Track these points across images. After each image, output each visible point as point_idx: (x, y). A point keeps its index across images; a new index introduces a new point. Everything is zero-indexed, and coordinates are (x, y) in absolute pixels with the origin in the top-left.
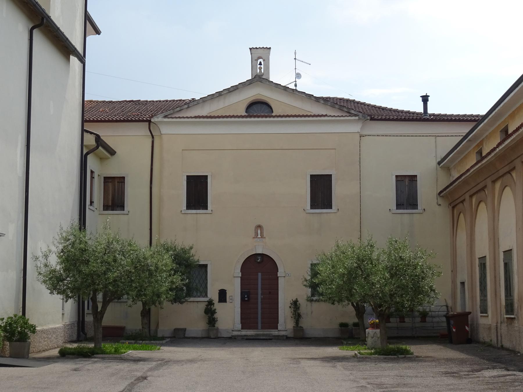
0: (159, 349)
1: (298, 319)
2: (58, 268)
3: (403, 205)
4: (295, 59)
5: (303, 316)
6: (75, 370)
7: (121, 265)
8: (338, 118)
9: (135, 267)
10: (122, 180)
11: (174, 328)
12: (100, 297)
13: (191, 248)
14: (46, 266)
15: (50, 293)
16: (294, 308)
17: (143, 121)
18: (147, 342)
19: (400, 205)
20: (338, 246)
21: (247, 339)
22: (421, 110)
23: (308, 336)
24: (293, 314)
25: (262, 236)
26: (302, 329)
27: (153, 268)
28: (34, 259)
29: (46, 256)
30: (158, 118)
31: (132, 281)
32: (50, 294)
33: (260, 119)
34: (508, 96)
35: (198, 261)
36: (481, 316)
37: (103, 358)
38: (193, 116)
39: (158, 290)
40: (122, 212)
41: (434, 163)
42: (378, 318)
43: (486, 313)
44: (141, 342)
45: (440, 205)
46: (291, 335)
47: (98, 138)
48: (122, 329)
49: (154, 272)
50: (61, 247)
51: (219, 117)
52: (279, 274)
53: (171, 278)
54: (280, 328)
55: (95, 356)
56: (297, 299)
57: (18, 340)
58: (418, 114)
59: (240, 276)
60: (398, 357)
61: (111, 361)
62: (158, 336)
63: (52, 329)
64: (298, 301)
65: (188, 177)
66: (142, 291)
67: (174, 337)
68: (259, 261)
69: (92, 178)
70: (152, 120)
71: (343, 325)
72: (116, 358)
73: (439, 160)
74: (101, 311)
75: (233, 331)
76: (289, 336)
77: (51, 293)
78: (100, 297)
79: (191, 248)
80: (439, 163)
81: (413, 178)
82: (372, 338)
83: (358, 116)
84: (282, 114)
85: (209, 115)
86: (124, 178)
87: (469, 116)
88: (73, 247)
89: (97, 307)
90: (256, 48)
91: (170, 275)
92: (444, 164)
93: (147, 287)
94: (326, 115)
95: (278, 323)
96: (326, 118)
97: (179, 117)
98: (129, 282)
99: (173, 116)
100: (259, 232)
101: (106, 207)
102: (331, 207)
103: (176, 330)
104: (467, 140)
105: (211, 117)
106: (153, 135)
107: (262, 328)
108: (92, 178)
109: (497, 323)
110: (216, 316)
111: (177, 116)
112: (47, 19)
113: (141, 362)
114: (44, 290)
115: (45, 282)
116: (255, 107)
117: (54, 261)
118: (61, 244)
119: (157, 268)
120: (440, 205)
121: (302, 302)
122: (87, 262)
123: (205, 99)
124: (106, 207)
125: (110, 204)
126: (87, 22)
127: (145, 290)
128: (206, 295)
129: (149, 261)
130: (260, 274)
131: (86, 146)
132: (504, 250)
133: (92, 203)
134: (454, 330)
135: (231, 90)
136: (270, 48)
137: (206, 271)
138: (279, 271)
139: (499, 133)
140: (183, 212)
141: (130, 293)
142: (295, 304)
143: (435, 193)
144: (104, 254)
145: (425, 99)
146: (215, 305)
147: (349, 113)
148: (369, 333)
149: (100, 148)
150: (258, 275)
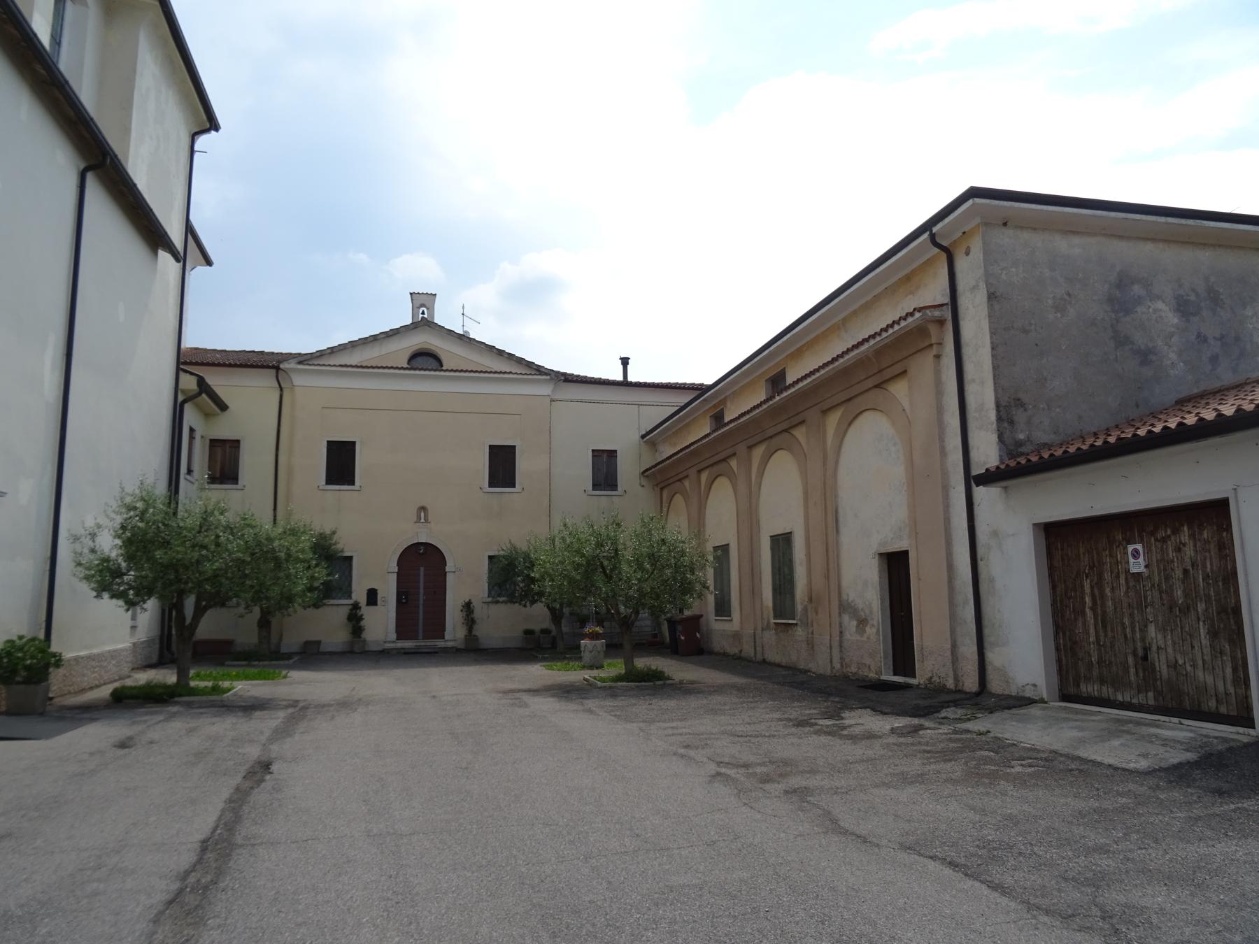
0: (285, 677)
1: (471, 626)
2: (114, 554)
3: (600, 485)
4: (463, 314)
5: (478, 621)
6: (123, 745)
7: (227, 550)
8: (525, 377)
9: (253, 554)
10: (235, 444)
11: (305, 640)
12: (190, 603)
13: (334, 533)
14: (93, 551)
15: (95, 597)
16: (466, 611)
17: (268, 367)
18: (266, 663)
19: (597, 485)
20: (565, 525)
21: (405, 653)
22: (620, 378)
23: (481, 647)
24: (465, 620)
25: (426, 521)
26: (476, 638)
27: (282, 555)
28: (71, 541)
29: (93, 536)
30: (289, 363)
31: (246, 576)
32: (95, 599)
33: (427, 373)
34: (800, 324)
35: (342, 551)
36: (716, 620)
37: (189, 705)
38: (337, 364)
39: (290, 590)
41: (637, 437)
43: (730, 616)
44: (256, 663)
45: (643, 486)
46: (462, 646)
47: (201, 381)
48: (228, 643)
49: (284, 562)
50: (119, 520)
51: (372, 367)
52: (447, 569)
53: (310, 572)
54: (447, 637)
55: (176, 699)
56: (470, 600)
57: (27, 681)
59: (397, 570)
60: (655, 684)
61: (202, 713)
62: (282, 651)
63: (109, 652)
64: (471, 603)
65: (331, 444)
66: (263, 593)
67: (304, 653)
68: (421, 551)
69: (192, 438)
70: (282, 366)
71: (528, 632)
72: (212, 705)
73: (644, 433)
74: (191, 624)
75: (385, 642)
76: (459, 647)
77: (98, 596)
78: (190, 603)
79: (334, 533)
80: (643, 437)
81: (612, 454)
82: (591, 652)
83: (550, 375)
84: (455, 369)
85: (359, 365)
86: (238, 441)
87: (674, 384)
88: (142, 520)
89: (184, 619)
90: (418, 293)
91: (309, 568)
92: (651, 437)
93: (270, 585)
94: (510, 373)
95: (445, 631)
96: (511, 376)
97: (319, 365)
98: (240, 578)
99: (310, 363)
100: (422, 514)
101: (213, 480)
102: (514, 486)
103: (307, 643)
104: (701, 399)
105: (362, 367)
106: (283, 386)
107: (425, 637)
108: (192, 438)
109: (755, 629)
110: (362, 623)
111: (316, 363)
112: (111, 159)
113: (258, 713)
114: (86, 590)
115: (87, 578)
116: (419, 359)
117: (109, 545)
118: (121, 514)
119: (289, 555)
120: (643, 486)
121: (476, 604)
122: (166, 544)
123: (355, 343)
124: (213, 480)
125: (218, 475)
126: (189, 235)
127: (268, 590)
128: (350, 597)
129: (276, 543)
130: (422, 569)
131: (183, 391)
132: (772, 535)
133: (189, 472)
134: (683, 638)
135: (390, 333)
136: (435, 295)
137: (351, 565)
138: (448, 564)
139: (763, 383)
140: (321, 488)
141: (243, 595)
142: (468, 607)
143: (637, 472)
144: (199, 532)
145: (625, 362)
146: (362, 609)
148: (586, 645)
149: (204, 395)
150: (420, 570)
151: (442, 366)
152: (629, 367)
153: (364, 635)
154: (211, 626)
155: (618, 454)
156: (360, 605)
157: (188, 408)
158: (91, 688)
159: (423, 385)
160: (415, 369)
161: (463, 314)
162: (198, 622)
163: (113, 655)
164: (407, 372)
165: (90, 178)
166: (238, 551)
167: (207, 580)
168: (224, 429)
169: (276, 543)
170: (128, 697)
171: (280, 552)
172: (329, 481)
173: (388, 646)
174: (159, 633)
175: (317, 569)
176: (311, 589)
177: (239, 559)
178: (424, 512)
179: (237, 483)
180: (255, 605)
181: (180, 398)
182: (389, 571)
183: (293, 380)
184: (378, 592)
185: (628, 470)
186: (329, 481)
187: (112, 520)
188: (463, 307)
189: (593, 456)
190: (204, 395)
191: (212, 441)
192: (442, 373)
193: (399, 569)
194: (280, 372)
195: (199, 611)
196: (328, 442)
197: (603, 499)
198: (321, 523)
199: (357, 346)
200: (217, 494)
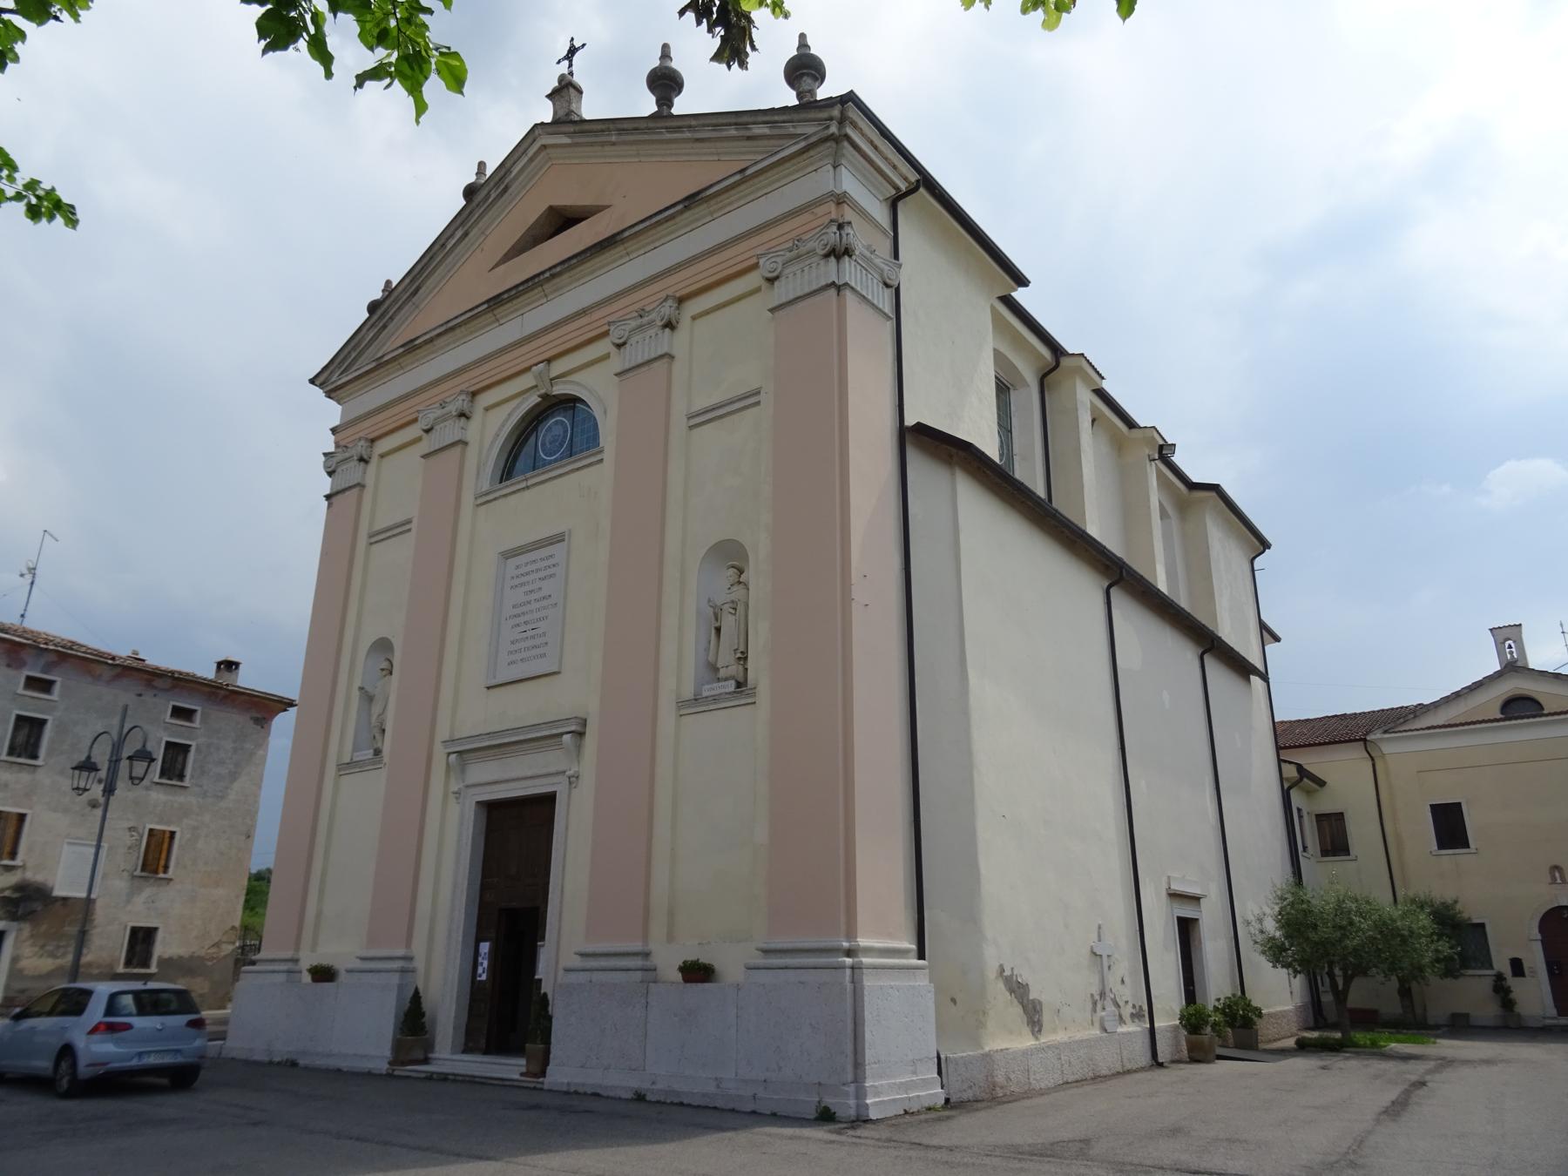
4: (1563, 632)
10: (1340, 816)
13: (1456, 902)
14: (1262, 932)
29: (1260, 921)
38: (1424, 726)
47: (1300, 768)
50: (1277, 909)
63: (1280, 1012)
69: (1300, 817)
70: (1368, 738)
75: (1544, 1018)
79: (1456, 902)
85: (1447, 723)
86: (1342, 814)
89: (1337, 987)
97: (1405, 731)
100: (1557, 875)
106: (1373, 755)
108: (1300, 817)
113: (1413, 1061)
114: (1265, 964)
117: (1271, 926)
123: (1437, 704)
125: (1330, 848)
128: (1491, 967)
131: (1287, 779)
133: (1305, 848)
136: (1520, 625)
140: (1434, 853)
149: (1305, 780)
151: (1542, 709)
153: (1518, 1009)
154: (1360, 994)
156: (682, 965)
157: (1294, 794)
158: (1275, 1040)
159: (1524, 734)
160: (1510, 719)
161: (1563, 632)
162: (1349, 987)
163: (1283, 1014)
164: (1502, 723)
165: (1206, 657)
166: (1369, 930)
167: (1349, 953)
168: (1326, 804)
169: (1399, 923)
170: (1310, 1046)
171: (1403, 930)
172: (1441, 846)
173: (1548, 1022)
174: (1308, 999)
175: (1440, 943)
176: (1438, 960)
177: (1370, 937)
178: (1559, 872)
179: (1349, 854)
180: (1392, 974)
181: (1286, 786)
182: (1531, 938)
183: (1383, 749)
184: (1524, 961)
186: (1441, 846)
187: (1272, 909)
188: (1561, 625)
190: (1305, 780)
191: (1318, 816)
192: (1544, 719)
193: (1542, 936)
194: (1368, 743)
195: (1348, 980)
196: (1431, 805)
198: (1441, 892)
199: (1439, 706)
200: (1335, 866)
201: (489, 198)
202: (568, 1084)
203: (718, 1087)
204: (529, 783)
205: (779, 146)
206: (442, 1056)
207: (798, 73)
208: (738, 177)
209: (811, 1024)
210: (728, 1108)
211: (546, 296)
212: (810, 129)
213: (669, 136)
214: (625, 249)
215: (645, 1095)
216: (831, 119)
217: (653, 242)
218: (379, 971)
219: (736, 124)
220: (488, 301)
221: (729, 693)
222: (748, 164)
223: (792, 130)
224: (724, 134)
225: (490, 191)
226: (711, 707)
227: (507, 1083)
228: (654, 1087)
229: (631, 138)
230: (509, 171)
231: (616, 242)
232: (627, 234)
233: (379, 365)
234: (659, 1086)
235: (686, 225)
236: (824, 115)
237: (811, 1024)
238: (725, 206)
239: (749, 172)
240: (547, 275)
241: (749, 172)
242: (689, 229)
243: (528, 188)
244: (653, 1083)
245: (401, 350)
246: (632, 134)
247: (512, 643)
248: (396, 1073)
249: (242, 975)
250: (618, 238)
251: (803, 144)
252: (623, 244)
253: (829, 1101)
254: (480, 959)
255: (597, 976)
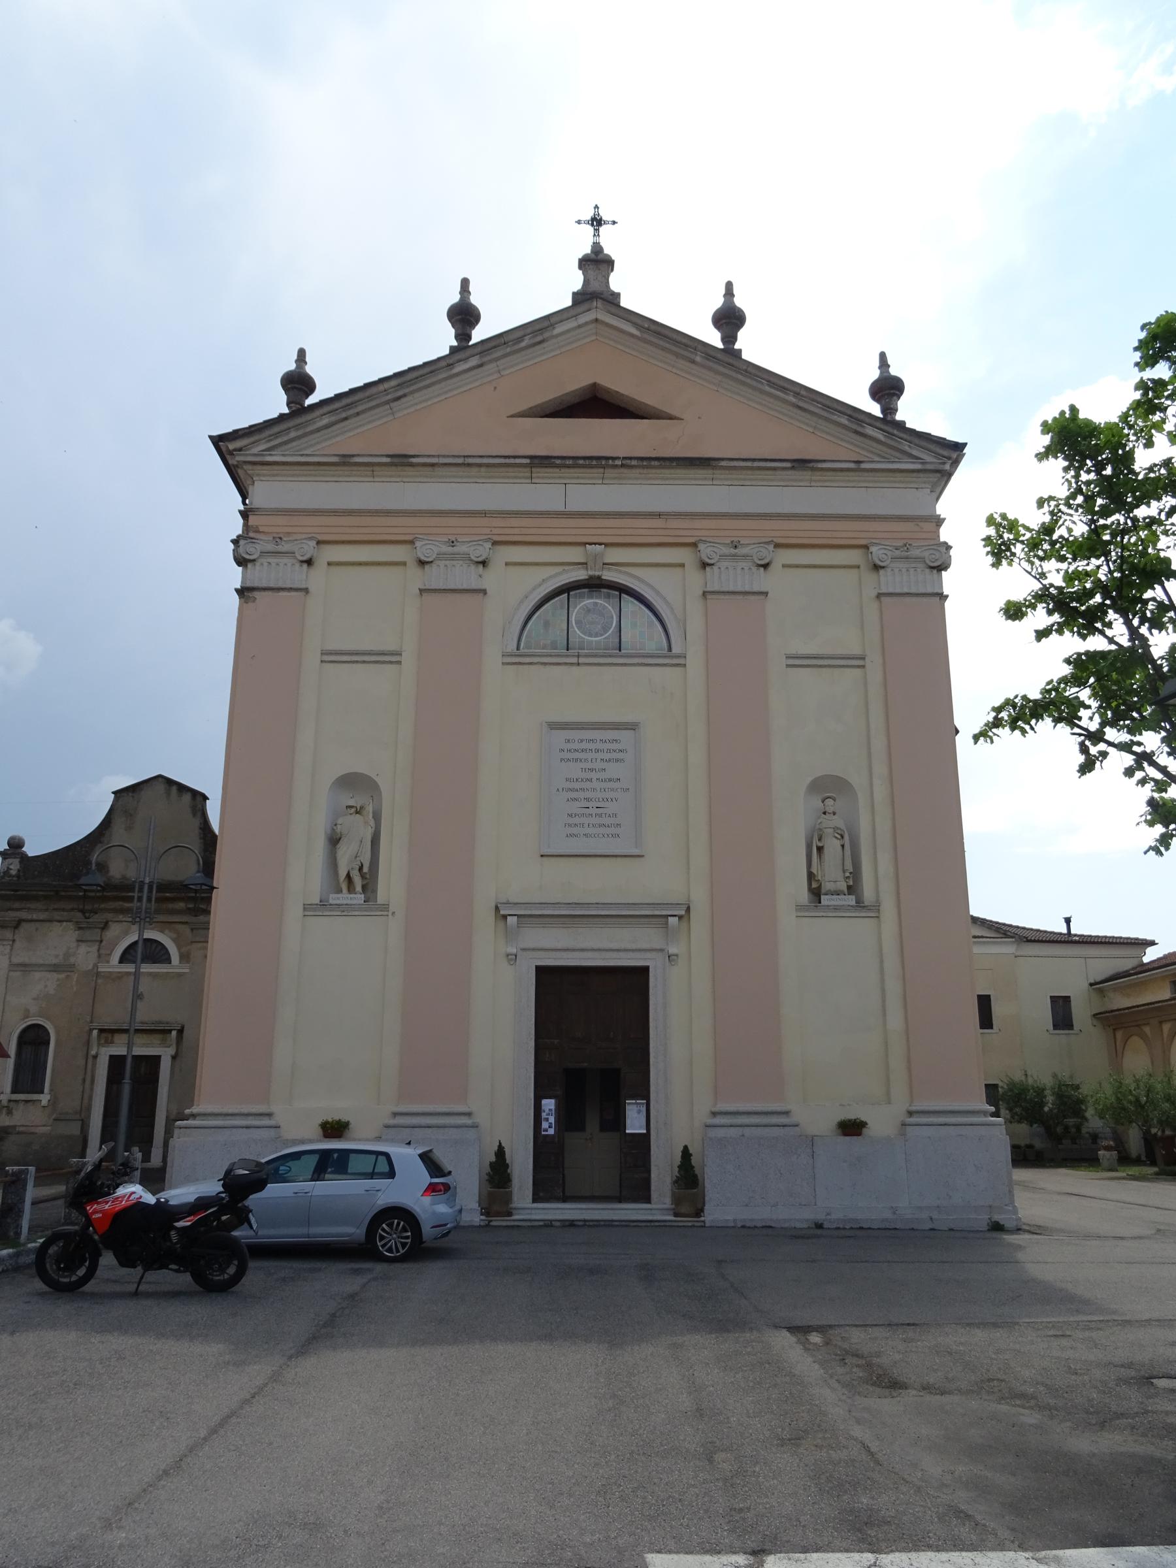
22: (1065, 931)
40: (1071, 1032)
42: (236, 1241)
54: (125, 1053)
58: (1061, 934)
73: (1092, 981)
81: (1067, 999)
82: (1108, 1160)
94: (982, 937)
145: (1068, 921)
147: (1005, 934)
152: (1072, 924)
155: (1072, 999)
179: (1073, 1029)
185: (1081, 1012)
186: (643, 972)
189: (1052, 1002)
197: (1062, 1035)
201: (520, 342)
202: (735, 1220)
203: (894, 1213)
204: (615, 955)
205: (897, 458)
206: (520, 1205)
207: (892, 392)
208: (852, 465)
209: (975, 1165)
210: (907, 1228)
211: (393, 414)
212: (928, 458)
213: (767, 389)
214: (714, 474)
215: (822, 1224)
216: (949, 458)
217: (745, 480)
218: (444, 1127)
219: (850, 416)
220: (531, 457)
221: (852, 906)
222: (866, 459)
223: (907, 448)
224: (835, 418)
225: (525, 336)
226: (831, 914)
227: (657, 1224)
228: (829, 1217)
229: (721, 369)
230: (552, 326)
231: (709, 465)
232: (723, 463)
233: (344, 462)
234: (833, 1217)
235: (783, 480)
236: (945, 453)
237: (975, 1165)
238: (825, 481)
239: (863, 466)
240: (619, 462)
241: (863, 466)
242: (783, 484)
243: (563, 350)
244: (828, 1214)
245: (388, 460)
246: (725, 367)
247: (570, 815)
248: (493, 1223)
249: (176, 1132)
250: (714, 463)
251: (918, 467)
252: (713, 469)
253: (997, 1217)
254: (544, 1115)
255: (747, 1131)
